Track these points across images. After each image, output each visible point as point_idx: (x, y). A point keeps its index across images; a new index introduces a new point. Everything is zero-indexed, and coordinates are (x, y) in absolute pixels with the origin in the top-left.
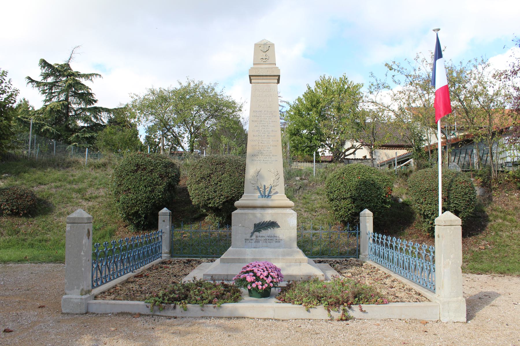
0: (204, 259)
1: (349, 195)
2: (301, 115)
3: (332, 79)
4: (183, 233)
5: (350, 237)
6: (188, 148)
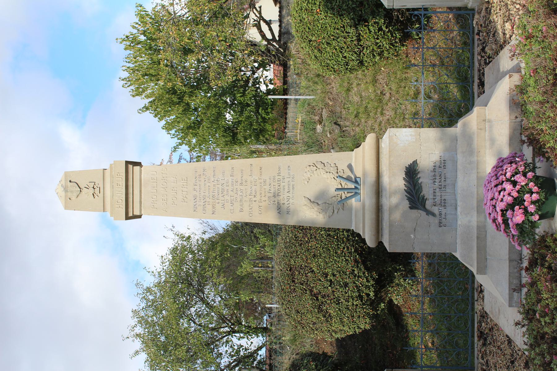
0: (476, 306)
1: (352, 31)
2: (198, 124)
3: (128, 65)
4: (426, 347)
5: (432, 28)
6: (261, 338)
